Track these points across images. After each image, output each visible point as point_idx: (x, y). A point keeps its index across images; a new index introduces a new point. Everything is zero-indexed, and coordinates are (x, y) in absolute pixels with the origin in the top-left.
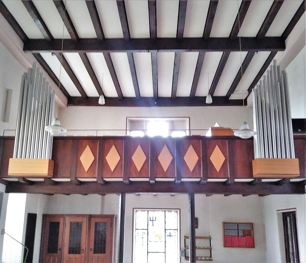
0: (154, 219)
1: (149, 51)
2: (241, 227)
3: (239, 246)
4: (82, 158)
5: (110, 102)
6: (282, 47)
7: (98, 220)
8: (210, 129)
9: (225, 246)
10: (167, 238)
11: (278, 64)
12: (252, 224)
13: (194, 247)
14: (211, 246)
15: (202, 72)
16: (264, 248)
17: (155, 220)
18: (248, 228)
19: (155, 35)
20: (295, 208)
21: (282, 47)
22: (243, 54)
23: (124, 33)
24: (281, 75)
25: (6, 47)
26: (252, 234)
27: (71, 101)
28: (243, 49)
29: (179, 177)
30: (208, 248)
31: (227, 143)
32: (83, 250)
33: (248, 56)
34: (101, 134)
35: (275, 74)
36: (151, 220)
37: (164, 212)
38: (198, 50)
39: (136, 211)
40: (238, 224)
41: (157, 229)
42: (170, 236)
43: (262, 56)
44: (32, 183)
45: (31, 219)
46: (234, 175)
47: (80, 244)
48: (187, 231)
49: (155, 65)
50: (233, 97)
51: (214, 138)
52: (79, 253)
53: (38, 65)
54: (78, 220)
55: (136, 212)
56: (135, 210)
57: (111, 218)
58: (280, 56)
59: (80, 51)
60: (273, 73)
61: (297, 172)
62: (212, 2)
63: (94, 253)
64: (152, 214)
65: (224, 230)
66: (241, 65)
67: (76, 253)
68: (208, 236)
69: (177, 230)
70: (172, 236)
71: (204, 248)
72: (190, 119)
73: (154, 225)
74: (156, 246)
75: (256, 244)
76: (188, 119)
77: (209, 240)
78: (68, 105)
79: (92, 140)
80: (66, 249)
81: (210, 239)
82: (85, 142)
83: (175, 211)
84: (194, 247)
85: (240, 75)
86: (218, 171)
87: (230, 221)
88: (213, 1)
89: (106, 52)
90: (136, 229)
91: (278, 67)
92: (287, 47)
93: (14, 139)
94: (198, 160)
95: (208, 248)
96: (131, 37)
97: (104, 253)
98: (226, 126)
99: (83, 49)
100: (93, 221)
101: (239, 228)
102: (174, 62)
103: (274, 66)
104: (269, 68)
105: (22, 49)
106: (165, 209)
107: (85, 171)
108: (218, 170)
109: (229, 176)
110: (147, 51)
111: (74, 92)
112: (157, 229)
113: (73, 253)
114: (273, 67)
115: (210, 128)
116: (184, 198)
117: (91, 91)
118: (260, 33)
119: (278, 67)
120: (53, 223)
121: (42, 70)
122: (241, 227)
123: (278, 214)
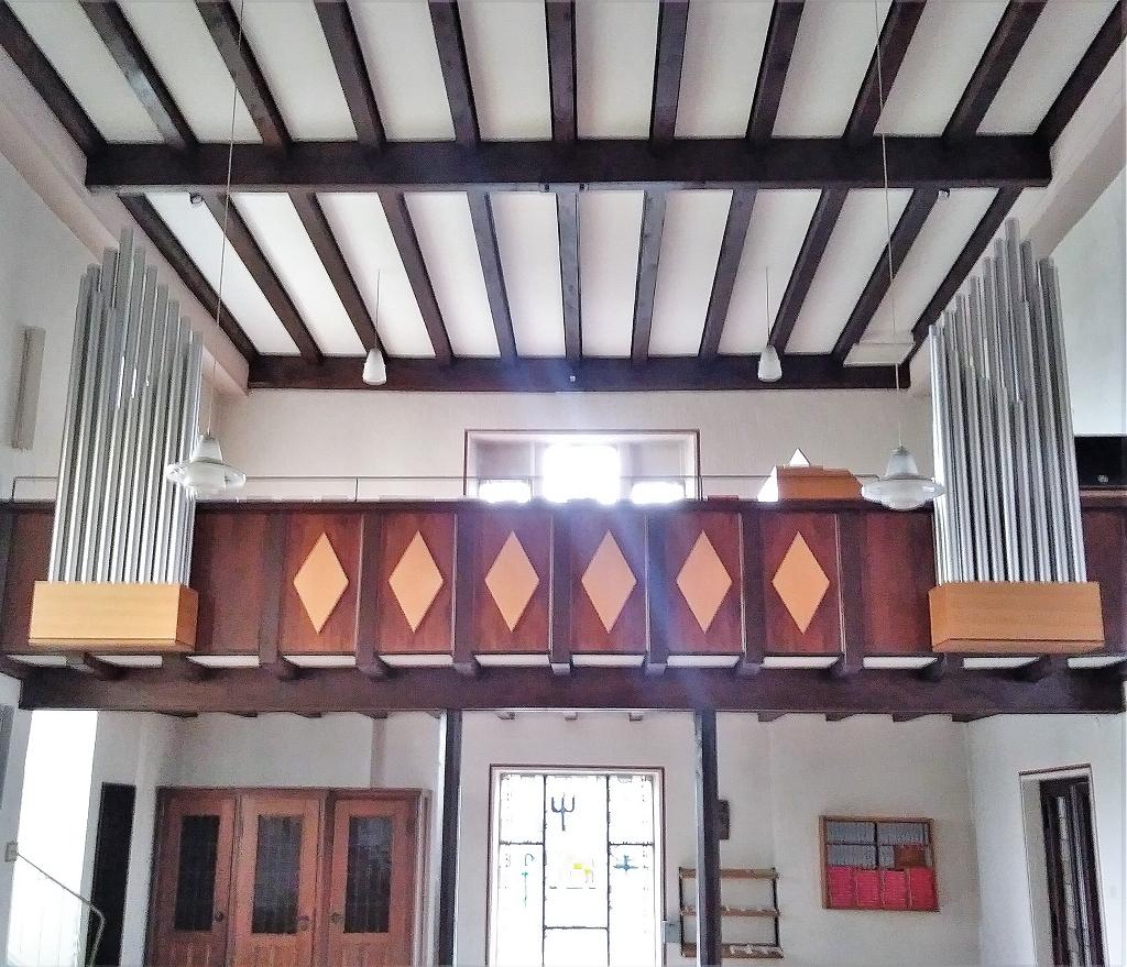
0: (568, 806)
1: (547, 189)
2: (888, 836)
3: (880, 906)
4: (303, 582)
5: (405, 374)
6: (1040, 172)
7: (360, 809)
8: (774, 473)
9: (828, 906)
10: (617, 874)
11: (1023, 234)
12: (927, 825)
13: (713, 910)
14: (776, 906)
15: (743, 263)
16: (974, 913)
17: (569, 808)
18: (914, 838)
19: (572, 129)
20: (1088, 766)
21: (1040, 172)
22: (896, 199)
23: (457, 120)
24: (1036, 275)
25: (24, 174)
26: (929, 862)
27: (263, 371)
28: (896, 181)
29: (660, 650)
30: (765, 913)
31: (837, 526)
32: (307, 918)
33: (912, 208)
34: (370, 493)
35: (1012, 274)
36: (554, 810)
37: (604, 779)
38: (729, 184)
39: (502, 776)
40: (876, 823)
41: (578, 841)
42: (627, 867)
43: (964, 205)
44: (119, 673)
45: (114, 804)
46: (860, 645)
47: (294, 896)
48: (690, 848)
49: (571, 238)
50: (859, 356)
51: (790, 507)
52: (292, 931)
53: (140, 239)
54: (288, 809)
55: (501, 779)
56: (497, 772)
57: (410, 800)
58: (1030, 205)
59: (296, 189)
60: (1005, 268)
61: (1095, 632)
62: (779, 9)
63: (348, 930)
64: (560, 786)
65: (827, 845)
66: (888, 240)
67: (280, 931)
68: (765, 866)
69: (653, 845)
70: (633, 867)
71: (751, 913)
72: (698, 438)
73: (566, 828)
74: (576, 903)
75: (941, 898)
76: (692, 437)
77: (768, 883)
78: (249, 387)
79: (340, 516)
80: (243, 916)
81: (774, 879)
82: (313, 521)
83: (646, 776)
84: (713, 910)
85: (882, 275)
86: (803, 629)
87: (847, 814)
88: (784, 4)
89: (392, 190)
90: (500, 843)
91: (1025, 248)
92: (1055, 174)
93: (52, 512)
94: (731, 589)
95: (765, 913)
96: (484, 135)
97: (384, 929)
98: (831, 464)
99: (307, 182)
100: (344, 811)
101: (881, 838)
102: (643, 229)
103: (1010, 244)
104: (989, 252)
105: (79, 180)
106: (608, 769)
107: (314, 629)
108: (803, 626)
109: (843, 648)
110: (543, 186)
111: (272, 337)
112: (578, 841)
113: (268, 930)
114: (1004, 246)
115: (775, 470)
116: (678, 728)
117: (335, 333)
118: (959, 122)
119: (1025, 248)
120: (196, 818)
121: (153, 258)
122: (888, 836)
123: (1024, 786)
